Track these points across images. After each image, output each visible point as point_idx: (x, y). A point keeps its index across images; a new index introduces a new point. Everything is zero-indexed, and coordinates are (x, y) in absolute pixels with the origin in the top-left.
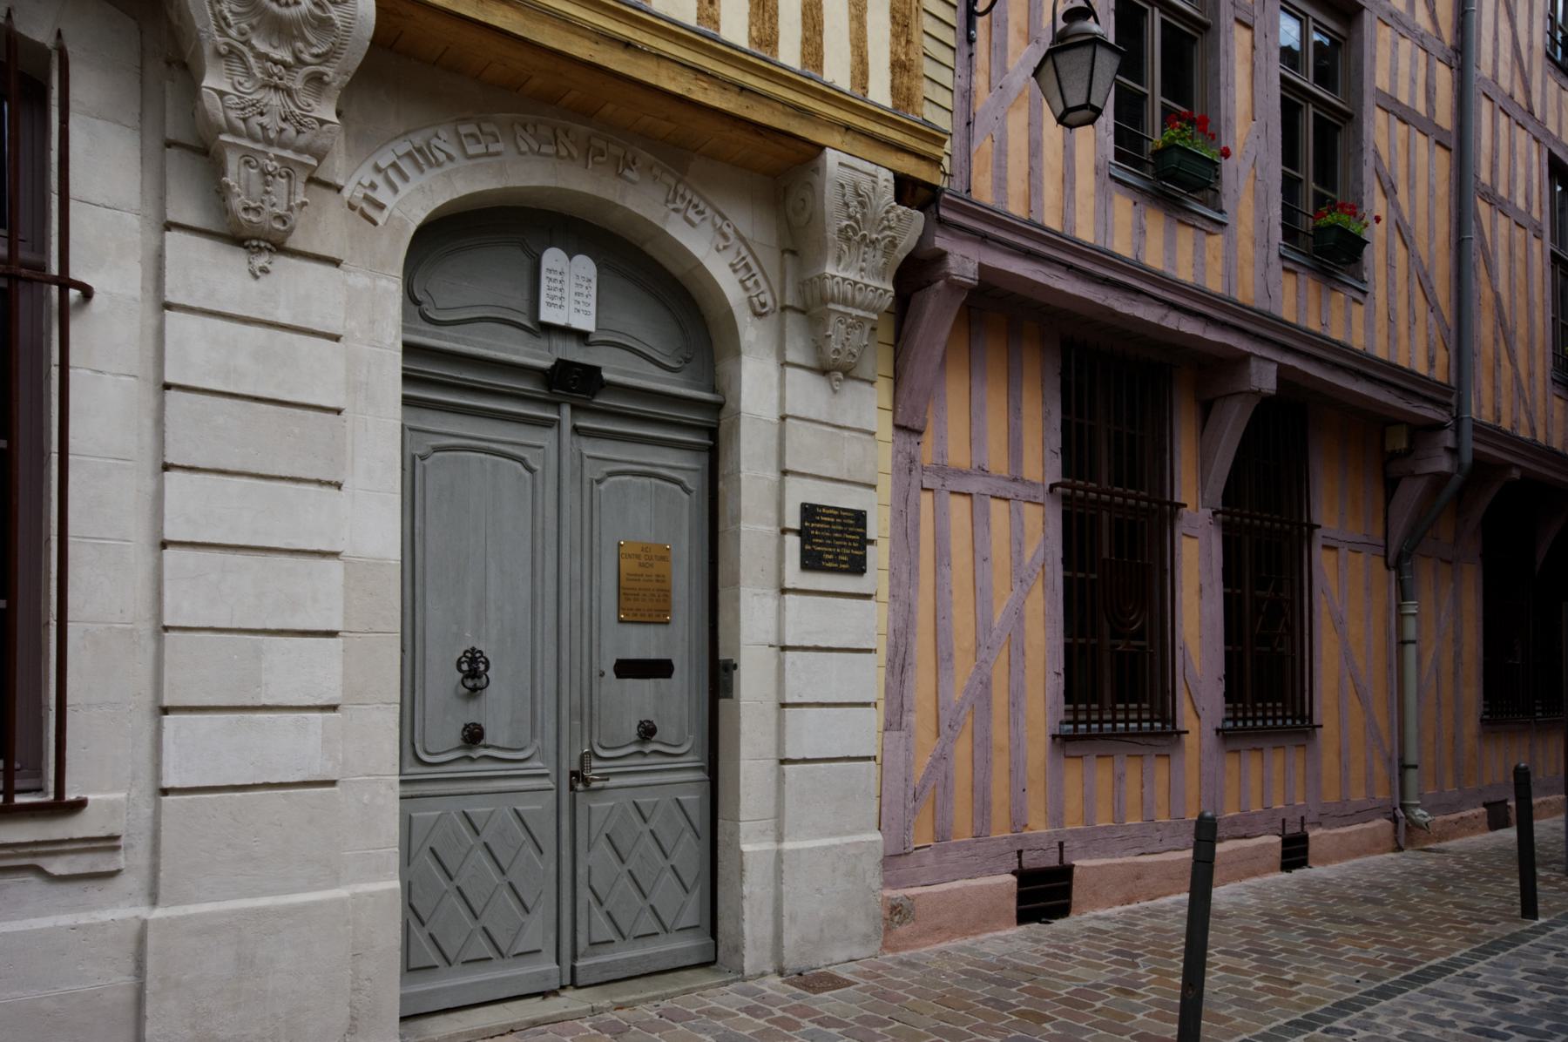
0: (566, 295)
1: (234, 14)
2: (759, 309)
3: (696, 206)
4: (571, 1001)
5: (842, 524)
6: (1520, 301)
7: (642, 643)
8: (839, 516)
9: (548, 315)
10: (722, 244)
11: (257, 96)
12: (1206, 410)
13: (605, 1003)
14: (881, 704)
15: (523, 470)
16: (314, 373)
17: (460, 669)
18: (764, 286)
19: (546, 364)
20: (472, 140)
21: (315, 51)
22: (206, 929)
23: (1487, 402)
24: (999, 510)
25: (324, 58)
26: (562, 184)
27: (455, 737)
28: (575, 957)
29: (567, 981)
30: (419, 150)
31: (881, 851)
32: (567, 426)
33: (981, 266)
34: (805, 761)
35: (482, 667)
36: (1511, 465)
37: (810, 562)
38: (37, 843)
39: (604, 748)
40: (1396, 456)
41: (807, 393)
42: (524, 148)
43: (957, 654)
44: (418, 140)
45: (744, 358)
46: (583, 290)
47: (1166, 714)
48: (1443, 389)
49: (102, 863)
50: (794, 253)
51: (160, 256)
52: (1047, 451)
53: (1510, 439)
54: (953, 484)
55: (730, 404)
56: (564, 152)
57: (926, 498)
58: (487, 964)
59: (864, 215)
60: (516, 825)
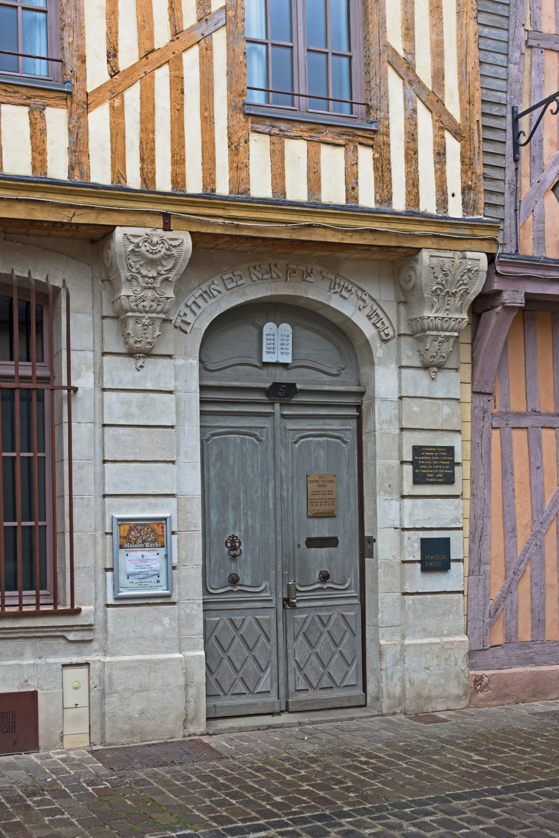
0: (276, 346)
1: (134, 262)
2: (384, 337)
3: (347, 288)
4: (284, 718)
5: (438, 456)
7: (321, 529)
8: (437, 451)
9: (266, 358)
10: (361, 304)
11: (142, 294)
13: (306, 720)
14: (467, 561)
15: (255, 441)
16: (163, 410)
17: (227, 546)
18: (387, 324)
19: (267, 385)
20: (230, 281)
21: (166, 269)
22: (128, 667)
25: (170, 271)
26: (274, 293)
27: (225, 579)
28: (287, 696)
29: (283, 708)
30: (205, 292)
31: (467, 646)
32: (277, 415)
33: (526, 294)
34: (418, 593)
35: (237, 544)
38: (64, 626)
39: (301, 586)
41: (419, 382)
42: (255, 278)
43: (518, 528)
44: (205, 287)
45: (376, 367)
46: (285, 342)
49: (86, 636)
50: (405, 303)
51: (101, 367)
54: (513, 422)
55: (369, 393)
56: (275, 276)
57: (496, 434)
58: (243, 696)
59: (447, 280)
60: (256, 626)
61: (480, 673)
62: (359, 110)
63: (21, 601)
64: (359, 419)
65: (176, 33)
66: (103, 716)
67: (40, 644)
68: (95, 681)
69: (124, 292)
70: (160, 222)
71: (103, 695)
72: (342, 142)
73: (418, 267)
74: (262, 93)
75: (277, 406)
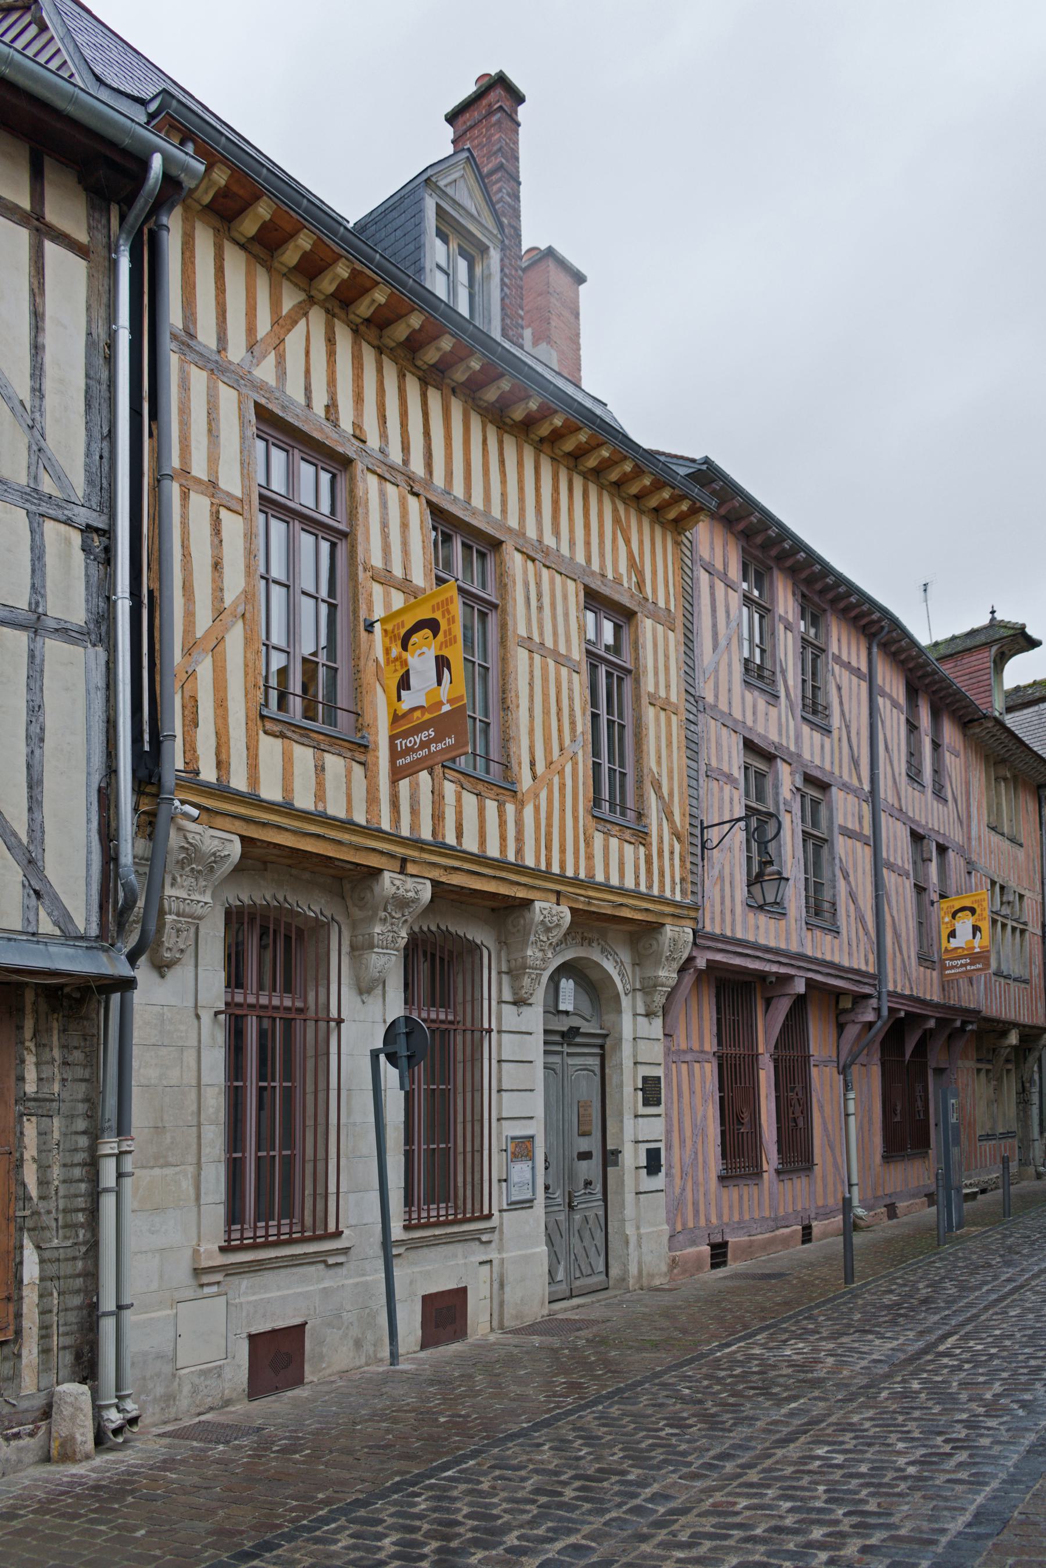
6: (903, 918)
7: (584, 1144)
19: (565, 1029)
23: (895, 982)
24: (697, 1065)
36: (900, 1010)
37: (646, 1103)
40: (845, 1011)
43: (169, 1171)
48: (872, 976)
52: (40, 864)
53: (902, 996)
62: (631, 815)
64: (603, 1057)
65: (219, 613)
66: (502, 1304)
68: (495, 1276)
69: (529, 953)
71: (502, 1285)
73: (661, 938)
74: (339, 705)
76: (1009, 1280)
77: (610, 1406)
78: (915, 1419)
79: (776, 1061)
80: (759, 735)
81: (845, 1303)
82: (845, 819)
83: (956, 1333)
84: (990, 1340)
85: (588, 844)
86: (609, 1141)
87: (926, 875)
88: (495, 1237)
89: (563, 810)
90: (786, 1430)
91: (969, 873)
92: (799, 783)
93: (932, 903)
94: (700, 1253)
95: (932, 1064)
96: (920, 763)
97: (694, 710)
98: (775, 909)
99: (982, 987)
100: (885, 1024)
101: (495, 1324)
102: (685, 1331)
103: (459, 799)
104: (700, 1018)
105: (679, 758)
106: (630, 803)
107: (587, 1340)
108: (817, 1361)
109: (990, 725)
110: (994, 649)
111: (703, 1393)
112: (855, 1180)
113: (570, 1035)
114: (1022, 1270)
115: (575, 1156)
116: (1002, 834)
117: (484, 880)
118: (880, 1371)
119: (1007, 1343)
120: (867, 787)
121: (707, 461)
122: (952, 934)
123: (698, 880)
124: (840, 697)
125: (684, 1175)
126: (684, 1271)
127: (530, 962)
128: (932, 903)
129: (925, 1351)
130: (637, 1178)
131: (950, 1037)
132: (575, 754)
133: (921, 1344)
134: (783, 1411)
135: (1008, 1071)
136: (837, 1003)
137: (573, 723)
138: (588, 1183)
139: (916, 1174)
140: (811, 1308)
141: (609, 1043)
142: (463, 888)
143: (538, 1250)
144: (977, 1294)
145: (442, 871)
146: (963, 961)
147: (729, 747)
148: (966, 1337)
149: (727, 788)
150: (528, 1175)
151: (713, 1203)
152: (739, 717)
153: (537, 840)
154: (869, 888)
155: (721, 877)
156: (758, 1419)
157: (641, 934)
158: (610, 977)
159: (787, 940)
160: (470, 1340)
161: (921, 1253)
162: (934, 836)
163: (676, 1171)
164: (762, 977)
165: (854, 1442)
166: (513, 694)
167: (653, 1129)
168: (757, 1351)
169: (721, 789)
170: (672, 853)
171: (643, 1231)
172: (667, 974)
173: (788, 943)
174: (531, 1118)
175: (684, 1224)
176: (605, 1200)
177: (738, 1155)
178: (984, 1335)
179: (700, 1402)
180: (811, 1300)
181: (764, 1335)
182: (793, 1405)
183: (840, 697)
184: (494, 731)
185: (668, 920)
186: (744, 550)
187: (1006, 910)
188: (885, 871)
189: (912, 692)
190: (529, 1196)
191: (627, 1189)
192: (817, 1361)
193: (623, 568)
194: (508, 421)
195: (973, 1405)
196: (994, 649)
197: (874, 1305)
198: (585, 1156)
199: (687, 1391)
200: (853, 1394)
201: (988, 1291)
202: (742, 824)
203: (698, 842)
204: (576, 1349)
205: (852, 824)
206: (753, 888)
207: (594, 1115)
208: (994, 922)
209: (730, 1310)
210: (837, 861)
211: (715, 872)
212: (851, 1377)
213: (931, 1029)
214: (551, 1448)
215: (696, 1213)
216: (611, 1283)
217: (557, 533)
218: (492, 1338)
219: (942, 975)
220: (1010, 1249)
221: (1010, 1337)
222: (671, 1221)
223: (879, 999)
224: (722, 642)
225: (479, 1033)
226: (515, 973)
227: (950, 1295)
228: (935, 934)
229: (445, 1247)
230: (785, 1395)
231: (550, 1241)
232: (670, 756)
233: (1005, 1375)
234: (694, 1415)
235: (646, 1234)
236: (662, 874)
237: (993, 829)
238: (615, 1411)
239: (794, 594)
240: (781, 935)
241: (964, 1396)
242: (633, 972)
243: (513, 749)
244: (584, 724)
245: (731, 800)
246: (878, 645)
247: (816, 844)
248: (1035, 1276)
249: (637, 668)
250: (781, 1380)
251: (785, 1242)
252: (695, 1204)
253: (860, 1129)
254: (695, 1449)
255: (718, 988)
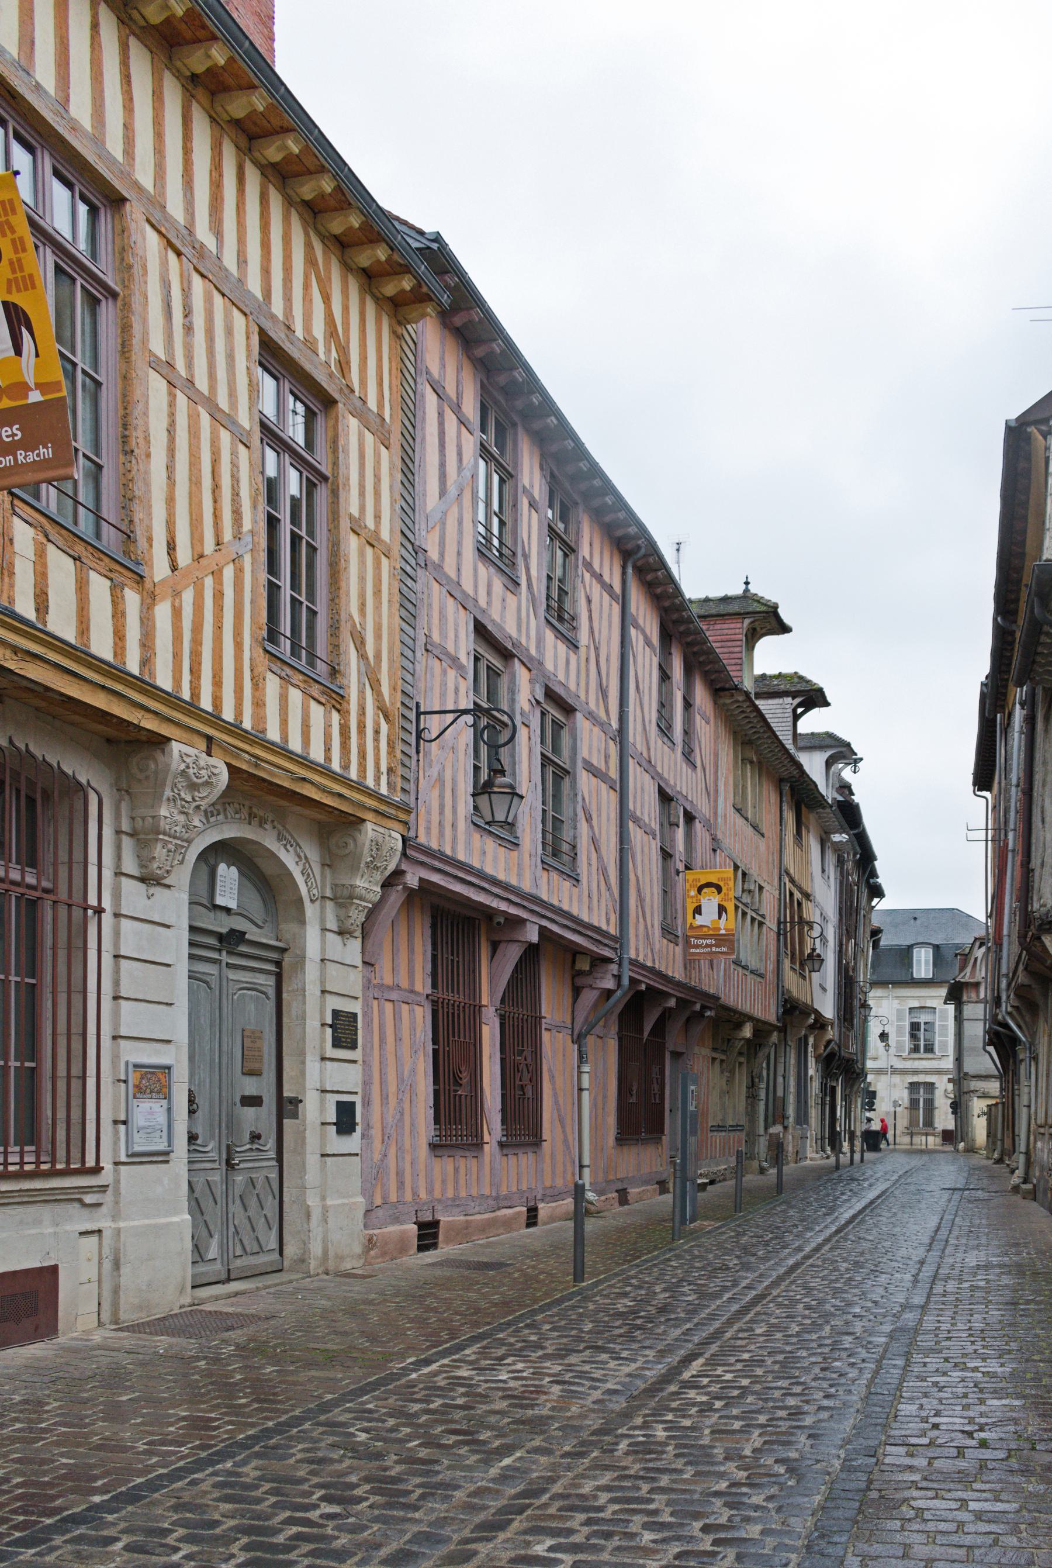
6: (647, 880)
7: (250, 1087)
12: (495, 946)
19: (224, 931)
23: (636, 949)
24: (405, 1007)
32: (224, 964)
33: (421, 879)
34: (334, 1155)
36: (640, 982)
37: (337, 1043)
40: (581, 973)
47: (478, 1134)
57: (375, 1002)
61: (371, 1232)
62: (321, 668)
63: (22, 1158)
64: (279, 977)
66: (116, 1291)
67: (58, 1208)
68: (106, 1251)
69: (164, 812)
70: (203, 746)
71: (117, 1265)
72: (323, 700)
73: (361, 838)
75: (224, 953)
76: (749, 1287)
77: (245, 1462)
78: (663, 1490)
79: (502, 1017)
80: (493, 621)
81: (573, 1307)
82: (590, 752)
83: (701, 1355)
84: (739, 1366)
85: (257, 684)
86: (286, 1087)
87: (673, 840)
88: (108, 1198)
89: (218, 628)
90: (495, 1504)
91: (714, 850)
92: (541, 697)
93: (678, 873)
94: (403, 1233)
95: (670, 1046)
96: (671, 717)
97: (413, 562)
98: (504, 831)
99: (722, 973)
100: (624, 995)
101: (106, 1316)
102: (373, 1338)
103: (41, 554)
104: (411, 950)
105: (390, 616)
106: (321, 650)
107: (238, 1346)
108: (539, 1391)
109: (741, 698)
110: (747, 622)
111: (385, 1440)
112: (586, 1161)
113: (232, 940)
114: (761, 1275)
115: (238, 1100)
116: (747, 819)
117: (86, 687)
118: (616, 1407)
119: (759, 1372)
120: (615, 725)
121: (438, 238)
122: (698, 910)
123: (412, 777)
124: (590, 611)
125: (385, 1138)
126: (384, 1254)
127: (163, 824)
128: (678, 873)
129: (666, 1379)
130: (323, 1137)
131: (688, 1020)
132: (240, 557)
133: (661, 1368)
134: (494, 1472)
135: (741, 1064)
136: (574, 962)
137: (237, 513)
138: (255, 1137)
139: (647, 1160)
140: (534, 1312)
141: (287, 960)
142: (47, 689)
143: (175, 1219)
144: (718, 1302)
145: (8, 653)
146: (708, 941)
147: (456, 625)
148: (713, 1362)
149: (452, 674)
150: (162, 1119)
151: (422, 1174)
152: (470, 591)
153: (177, 656)
154: (614, 840)
155: (440, 780)
156: (457, 1487)
157: (333, 827)
158: (290, 874)
159: (519, 875)
160: (61, 1340)
161: (656, 1248)
162: (682, 801)
163: (376, 1133)
164: (489, 914)
165: (586, 1530)
166: (140, 434)
167: (346, 1077)
168: (464, 1373)
169: (444, 673)
170: (377, 732)
171: (329, 1202)
172: (367, 885)
173: (520, 881)
174: (168, 1042)
175: (385, 1198)
176: (280, 1159)
177: (454, 1120)
178: (732, 1360)
179: (379, 1456)
180: (535, 1301)
181: (475, 1348)
182: (507, 1461)
183: (590, 611)
184: (108, 478)
185: (369, 816)
186: (483, 386)
187: (746, 899)
188: (631, 823)
189: (666, 636)
190: (162, 1146)
191: (309, 1149)
192: (539, 1391)
193: (319, 330)
194: (135, 15)
195: (731, 1466)
196: (747, 622)
197: (606, 1311)
198: (253, 1101)
199: (363, 1436)
200: (583, 1443)
201: (731, 1299)
202: (469, 719)
203: (413, 728)
204: (217, 1360)
205: (597, 761)
206: (479, 799)
207: (266, 1050)
208: (737, 908)
209: (435, 1310)
210: (579, 798)
211: (434, 772)
212: (582, 1416)
213: (670, 1009)
214: (127, 1548)
215: (401, 1185)
216: (286, 1264)
217: (217, 231)
218: (97, 1337)
219: (685, 952)
220: (746, 1250)
221: (761, 1363)
222: (367, 1192)
223: (620, 965)
224: (452, 490)
225: (81, 912)
226: (144, 836)
227: (689, 1303)
228: (679, 906)
229: (21, 1209)
230: (497, 1443)
231: (196, 1207)
232: (378, 607)
233: (762, 1419)
234: (367, 1480)
235: (337, 1204)
236: (362, 755)
237: (738, 810)
238: (250, 1471)
239: (542, 469)
240: (512, 867)
241: (719, 1452)
242: (323, 874)
243: (138, 515)
244: (254, 522)
245: (457, 690)
246: (634, 567)
247: (557, 773)
248: (775, 1284)
249: (336, 477)
250: (493, 1419)
251: (507, 1224)
252: (400, 1174)
253: (594, 1105)
254: (359, 1546)
255: (434, 918)
